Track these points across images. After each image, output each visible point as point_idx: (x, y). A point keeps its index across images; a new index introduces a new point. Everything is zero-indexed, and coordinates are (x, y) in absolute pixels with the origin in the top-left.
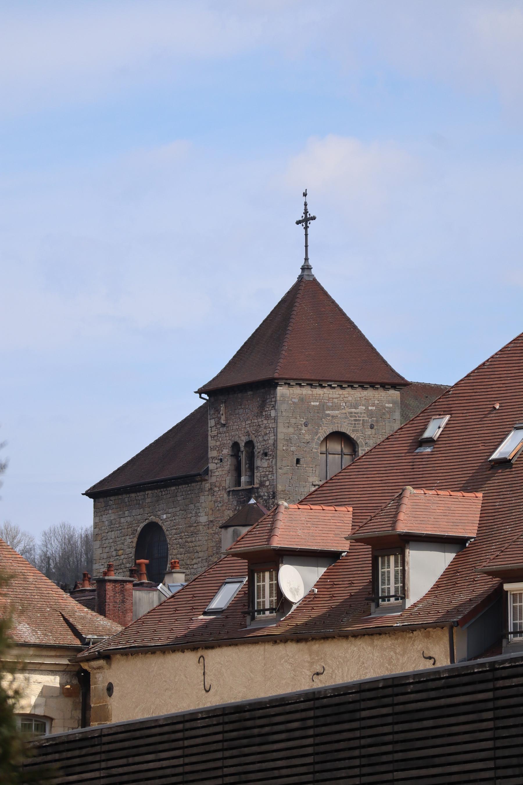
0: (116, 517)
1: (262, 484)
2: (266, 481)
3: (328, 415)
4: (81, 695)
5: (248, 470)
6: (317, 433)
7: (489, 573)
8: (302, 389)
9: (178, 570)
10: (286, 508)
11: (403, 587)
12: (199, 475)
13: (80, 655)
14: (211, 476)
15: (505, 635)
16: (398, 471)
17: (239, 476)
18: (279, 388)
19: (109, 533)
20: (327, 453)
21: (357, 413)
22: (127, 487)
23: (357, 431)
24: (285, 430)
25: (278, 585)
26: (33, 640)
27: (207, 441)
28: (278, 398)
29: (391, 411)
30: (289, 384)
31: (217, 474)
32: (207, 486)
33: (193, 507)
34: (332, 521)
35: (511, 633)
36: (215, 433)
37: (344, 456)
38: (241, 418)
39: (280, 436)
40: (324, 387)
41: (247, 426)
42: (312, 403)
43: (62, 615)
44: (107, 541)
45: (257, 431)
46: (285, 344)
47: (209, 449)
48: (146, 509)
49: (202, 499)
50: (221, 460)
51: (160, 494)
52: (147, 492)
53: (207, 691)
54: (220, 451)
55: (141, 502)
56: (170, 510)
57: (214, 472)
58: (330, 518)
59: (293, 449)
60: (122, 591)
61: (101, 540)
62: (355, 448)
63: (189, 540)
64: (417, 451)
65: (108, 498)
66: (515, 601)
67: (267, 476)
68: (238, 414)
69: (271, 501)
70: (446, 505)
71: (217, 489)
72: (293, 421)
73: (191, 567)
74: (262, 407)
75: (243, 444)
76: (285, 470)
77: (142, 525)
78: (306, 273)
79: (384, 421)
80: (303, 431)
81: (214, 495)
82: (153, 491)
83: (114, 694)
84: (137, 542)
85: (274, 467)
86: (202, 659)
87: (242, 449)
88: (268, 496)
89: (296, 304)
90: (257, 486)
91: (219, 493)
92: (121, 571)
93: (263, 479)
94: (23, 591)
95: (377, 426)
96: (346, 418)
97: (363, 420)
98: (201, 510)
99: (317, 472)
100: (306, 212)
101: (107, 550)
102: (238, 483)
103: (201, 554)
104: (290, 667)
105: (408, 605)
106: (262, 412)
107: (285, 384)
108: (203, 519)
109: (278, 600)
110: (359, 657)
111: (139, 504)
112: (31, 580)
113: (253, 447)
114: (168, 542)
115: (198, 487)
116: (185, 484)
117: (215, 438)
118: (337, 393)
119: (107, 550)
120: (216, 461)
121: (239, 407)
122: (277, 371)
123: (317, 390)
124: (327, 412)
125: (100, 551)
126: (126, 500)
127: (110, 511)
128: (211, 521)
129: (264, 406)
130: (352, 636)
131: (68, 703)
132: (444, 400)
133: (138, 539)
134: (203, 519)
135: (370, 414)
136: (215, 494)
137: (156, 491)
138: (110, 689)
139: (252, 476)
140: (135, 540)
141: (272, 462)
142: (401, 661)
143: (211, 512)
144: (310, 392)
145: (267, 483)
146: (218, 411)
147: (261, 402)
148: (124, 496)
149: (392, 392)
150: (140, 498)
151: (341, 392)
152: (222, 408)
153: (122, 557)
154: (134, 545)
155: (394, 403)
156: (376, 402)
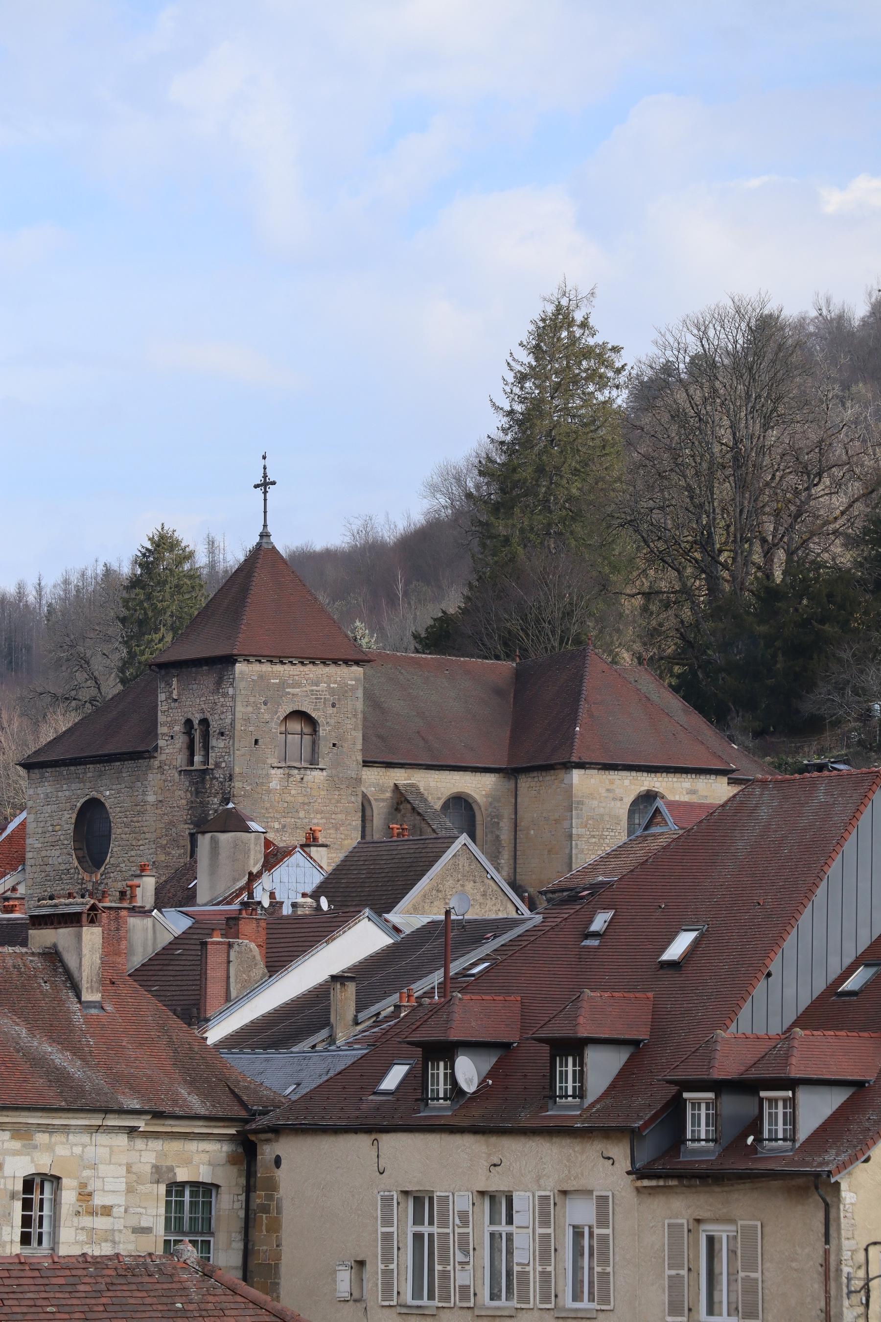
0: (52, 790)
1: (217, 765)
2: (222, 762)
3: (289, 693)
4: (245, 1162)
5: (202, 749)
6: (276, 712)
7: (670, 1082)
8: (261, 665)
9: (148, 873)
10: (460, 999)
11: (581, 1087)
12: (148, 751)
13: (248, 1127)
14: (161, 753)
15: (684, 1141)
16: (565, 963)
17: (192, 755)
18: (237, 665)
19: (45, 807)
20: (286, 733)
21: (319, 691)
22: (67, 759)
23: (318, 710)
24: (243, 710)
25: (453, 1075)
26: (203, 1112)
27: (156, 717)
28: (237, 676)
29: (354, 689)
30: (248, 661)
31: (167, 751)
32: (156, 763)
33: (140, 785)
34: (503, 1011)
35: (689, 1140)
36: (165, 708)
37: (304, 736)
38: (196, 695)
39: (238, 715)
40: (285, 663)
41: (201, 703)
42: (272, 681)
43: (228, 1085)
44: (42, 815)
45: (212, 709)
46: (245, 617)
47: (159, 724)
48: (87, 784)
49: (150, 777)
50: (172, 737)
51: (103, 769)
52: (88, 766)
53: (381, 1173)
54: (171, 727)
55: (81, 776)
56: (114, 787)
57: (164, 750)
58: (500, 1008)
59: (251, 729)
60: (117, 919)
61: (36, 813)
62: (316, 728)
63: (135, 819)
64: (583, 944)
65: (44, 769)
66: (693, 1109)
67: (223, 757)
68: (192, 689)
69: (227, 784)
70: (621, 1007)
71: (167, 767)
72: (252, 699)
73: (136, 848)
74: (219, 683)
75: (197, 722)
76: (243, 750)
77: (82, 801)
78: (265, 540)
79: (347, 699)
80: (262, 711)
81: (163, 774)
82: (95, 766)
83: (282, 1166)
84: (77, 818)
85: (232, 748)
86: (375, 1142)
87: (196, 726)
88: (224, 778)
89: (256, 574)
90: (213, 767)
91: (170, 772)
92: (58, 847)
93: (218, 760)
94: (190, 1061)
95: (339, 704)
96: (307, 696)
97: (325, 698)
98: (149, 789)
99: (276, 754)
100: (265, 476)
101: (42, 824)
102: (191, 762)
103: (147, 836)
104: (466, 1157)
105: (586, 1105)
106: (218, 689)
107: (244, 660)
108: (151, 798)
109: (452, 1090)
110: (537, 1152)
111: (79, 778)
112: (196, 1049)
113: (208, 725)
114: (112, 820)
115: (146, 764)
116: (131, 760)
117: (166, 714)
118: (298, 670)
119: (42, 824)
120: (167, 738)
121: (193, 682)
122: (237, 647)
123: (277, 666)
124: (287, 690)
125: (34, 825)
126: (65, 773)
127: (46, 784)
128: (160, 801)
129: (221, 683)
130: (531, 1132)
131: (233, 1171)
132: (609, 893)
133: (78, 815)
134: (151, 798)
135: (332, 692)
136: (165, 772)
137: (98, 766)
138: (278, 1162)
139: (207, 756)
140: (74, 816)
141: (229, 743)
142: (580, 1159)
143: (160, 791)
144: (270, 669)
145: (223, 765)
146: (169, 685)
147: (217, 678)
148: (63, 768)
149: (355, 668)
150: (80, 771)
151: (302, 668)
152: (175, 681)
153: (60, 833)
154: (73, 821)
155: (356, 680)
156: (339, 679)
